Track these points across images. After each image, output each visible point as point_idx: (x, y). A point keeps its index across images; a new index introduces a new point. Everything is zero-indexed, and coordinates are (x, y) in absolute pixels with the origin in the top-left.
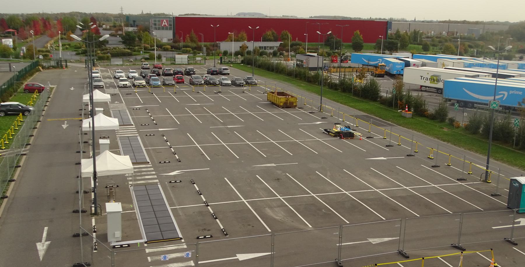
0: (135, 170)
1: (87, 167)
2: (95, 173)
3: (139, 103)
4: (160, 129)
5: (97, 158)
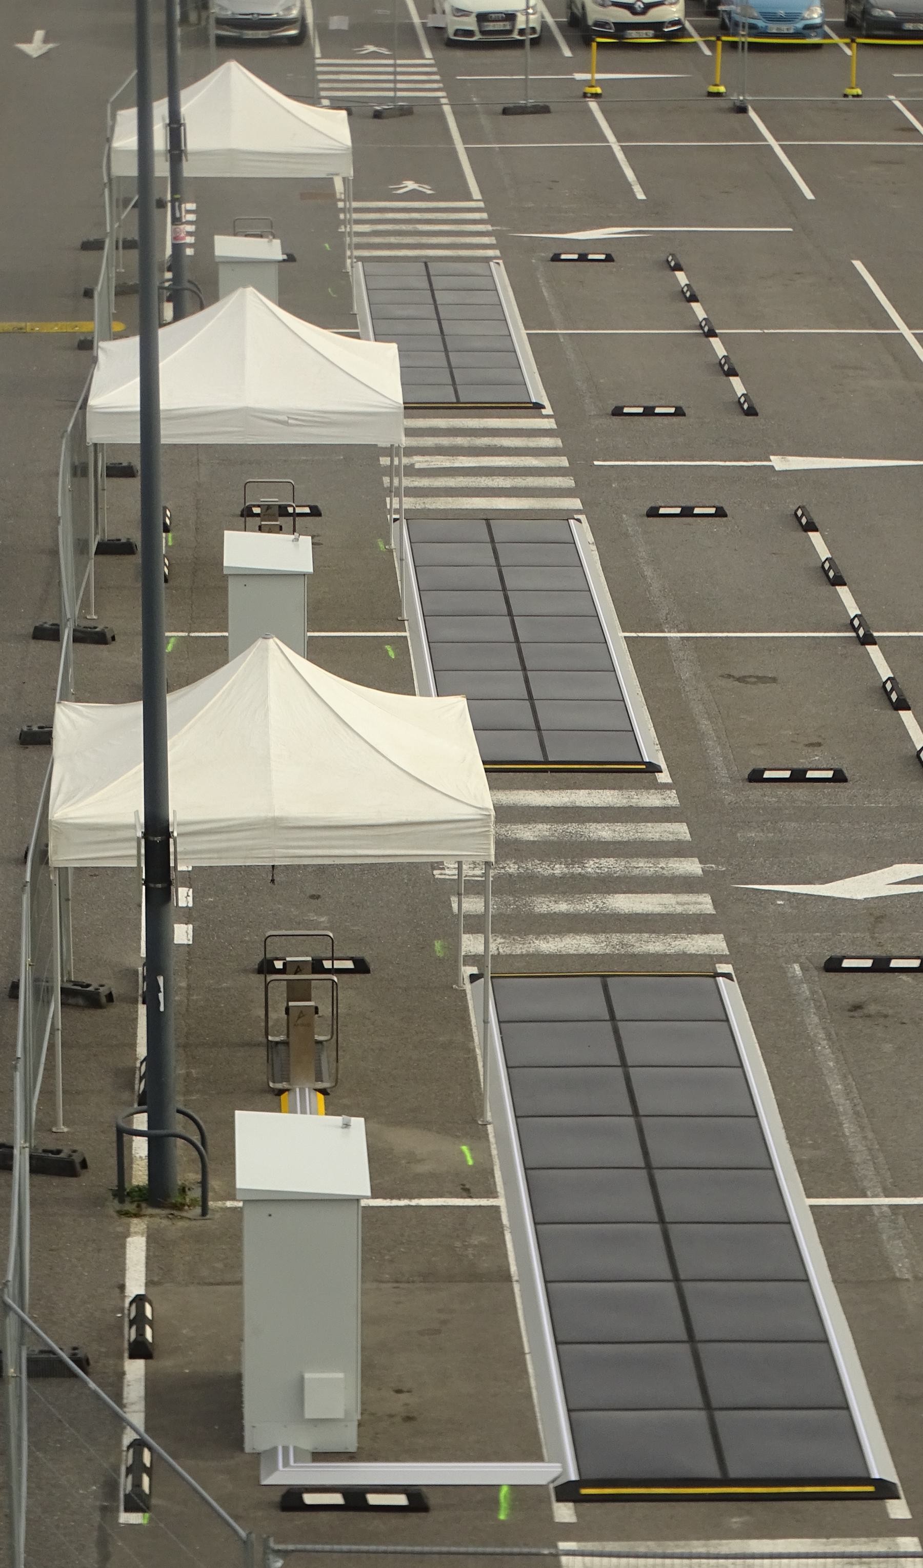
0: (527, 833)
1: (91, 783)
2: (157, 832)
3: (608, 201)
4: (779, 463)
5: (175, 704)
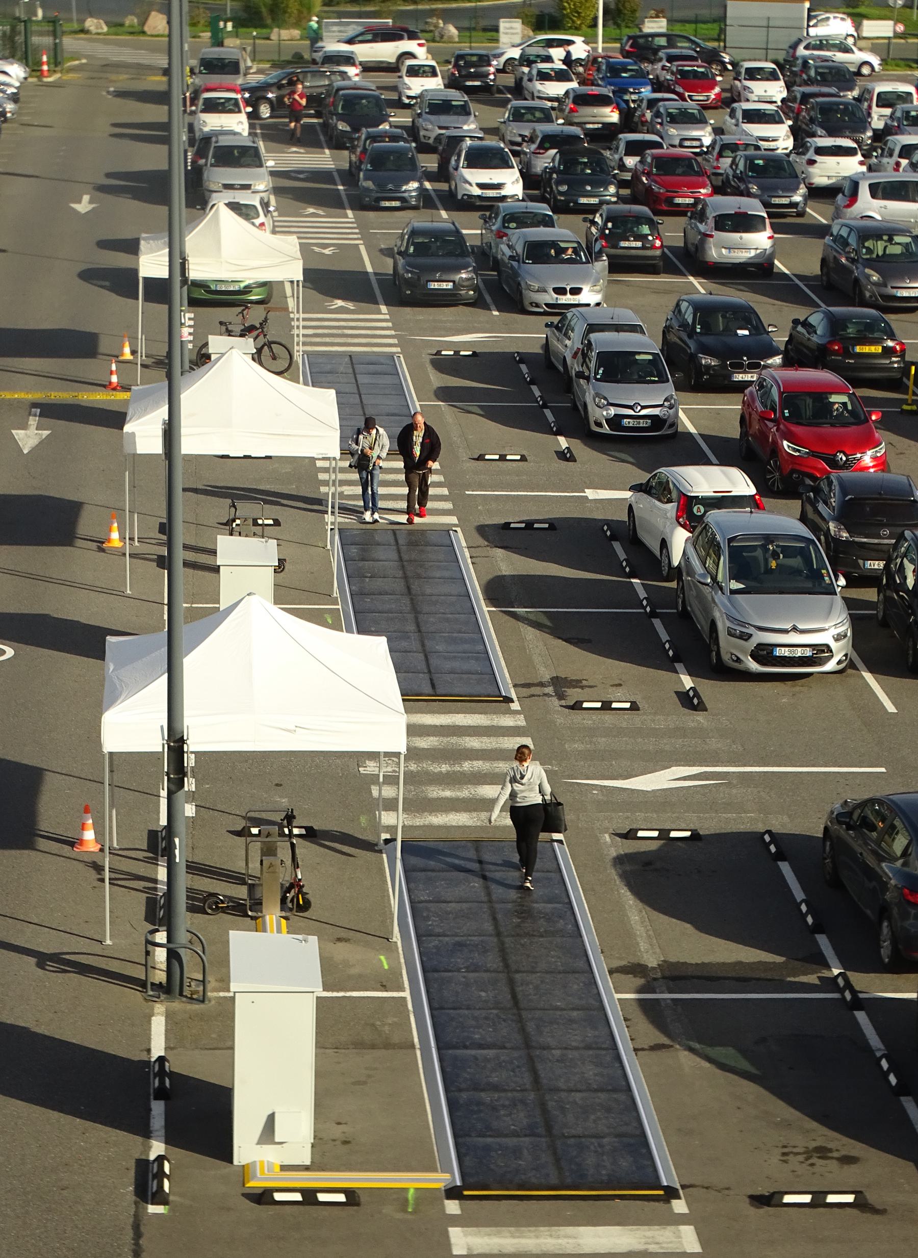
0: (424, 743)
2: (176, 742)
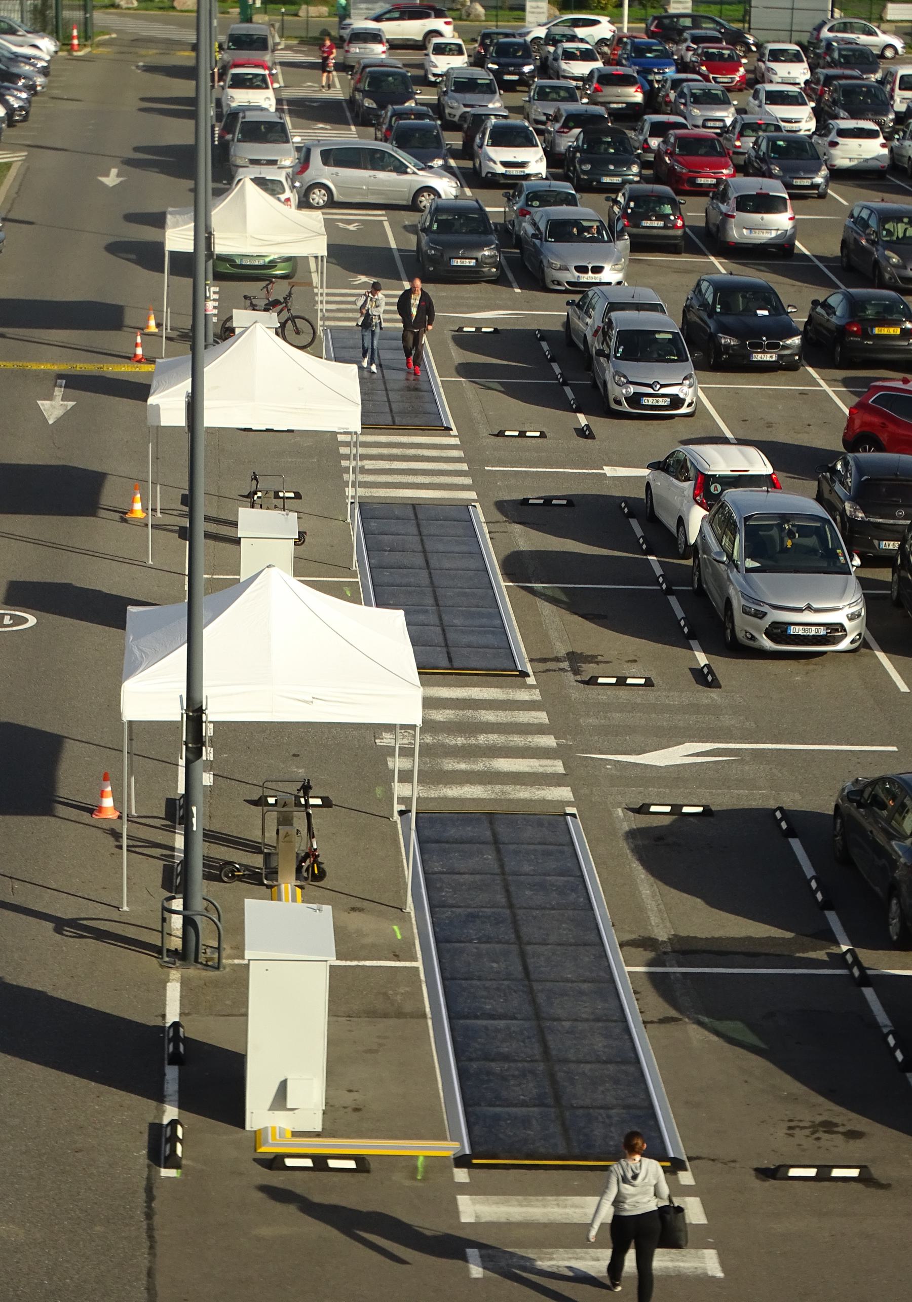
0: (440, 716)
2: (195, 712)
